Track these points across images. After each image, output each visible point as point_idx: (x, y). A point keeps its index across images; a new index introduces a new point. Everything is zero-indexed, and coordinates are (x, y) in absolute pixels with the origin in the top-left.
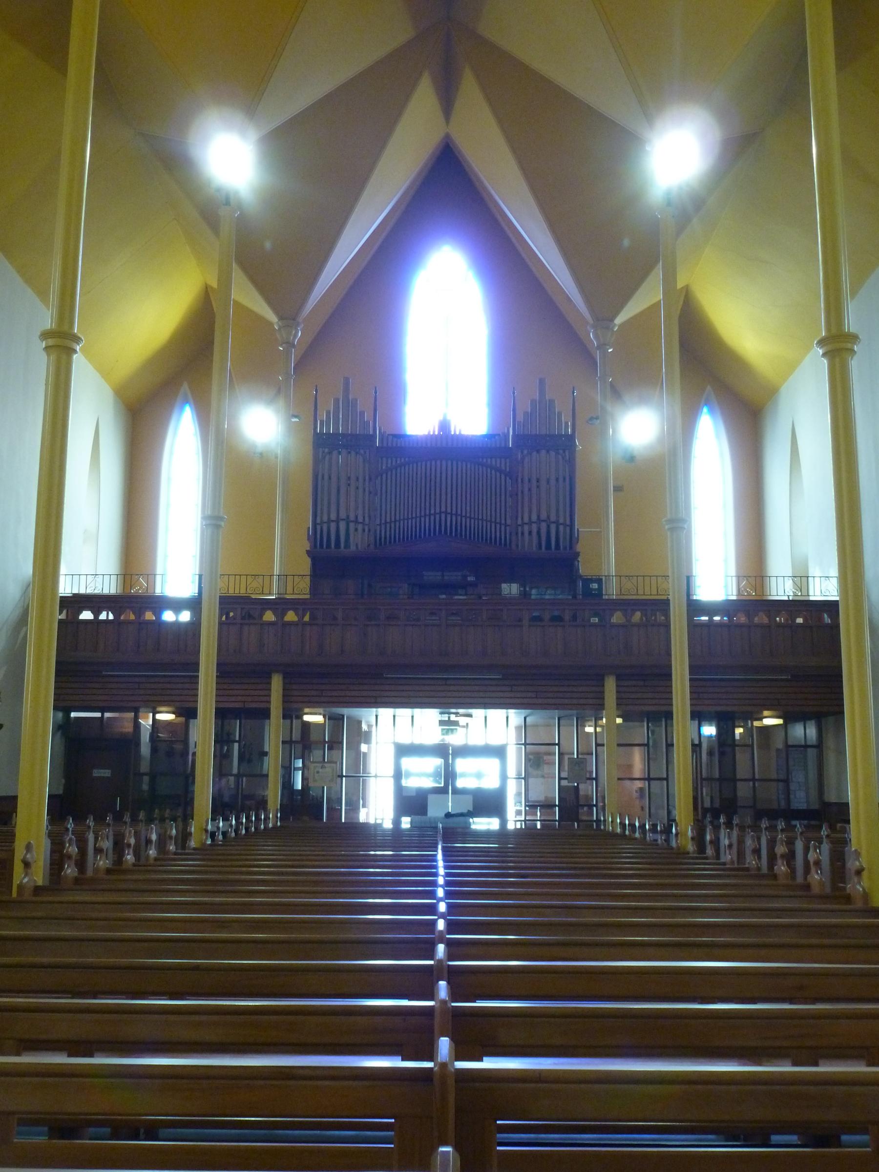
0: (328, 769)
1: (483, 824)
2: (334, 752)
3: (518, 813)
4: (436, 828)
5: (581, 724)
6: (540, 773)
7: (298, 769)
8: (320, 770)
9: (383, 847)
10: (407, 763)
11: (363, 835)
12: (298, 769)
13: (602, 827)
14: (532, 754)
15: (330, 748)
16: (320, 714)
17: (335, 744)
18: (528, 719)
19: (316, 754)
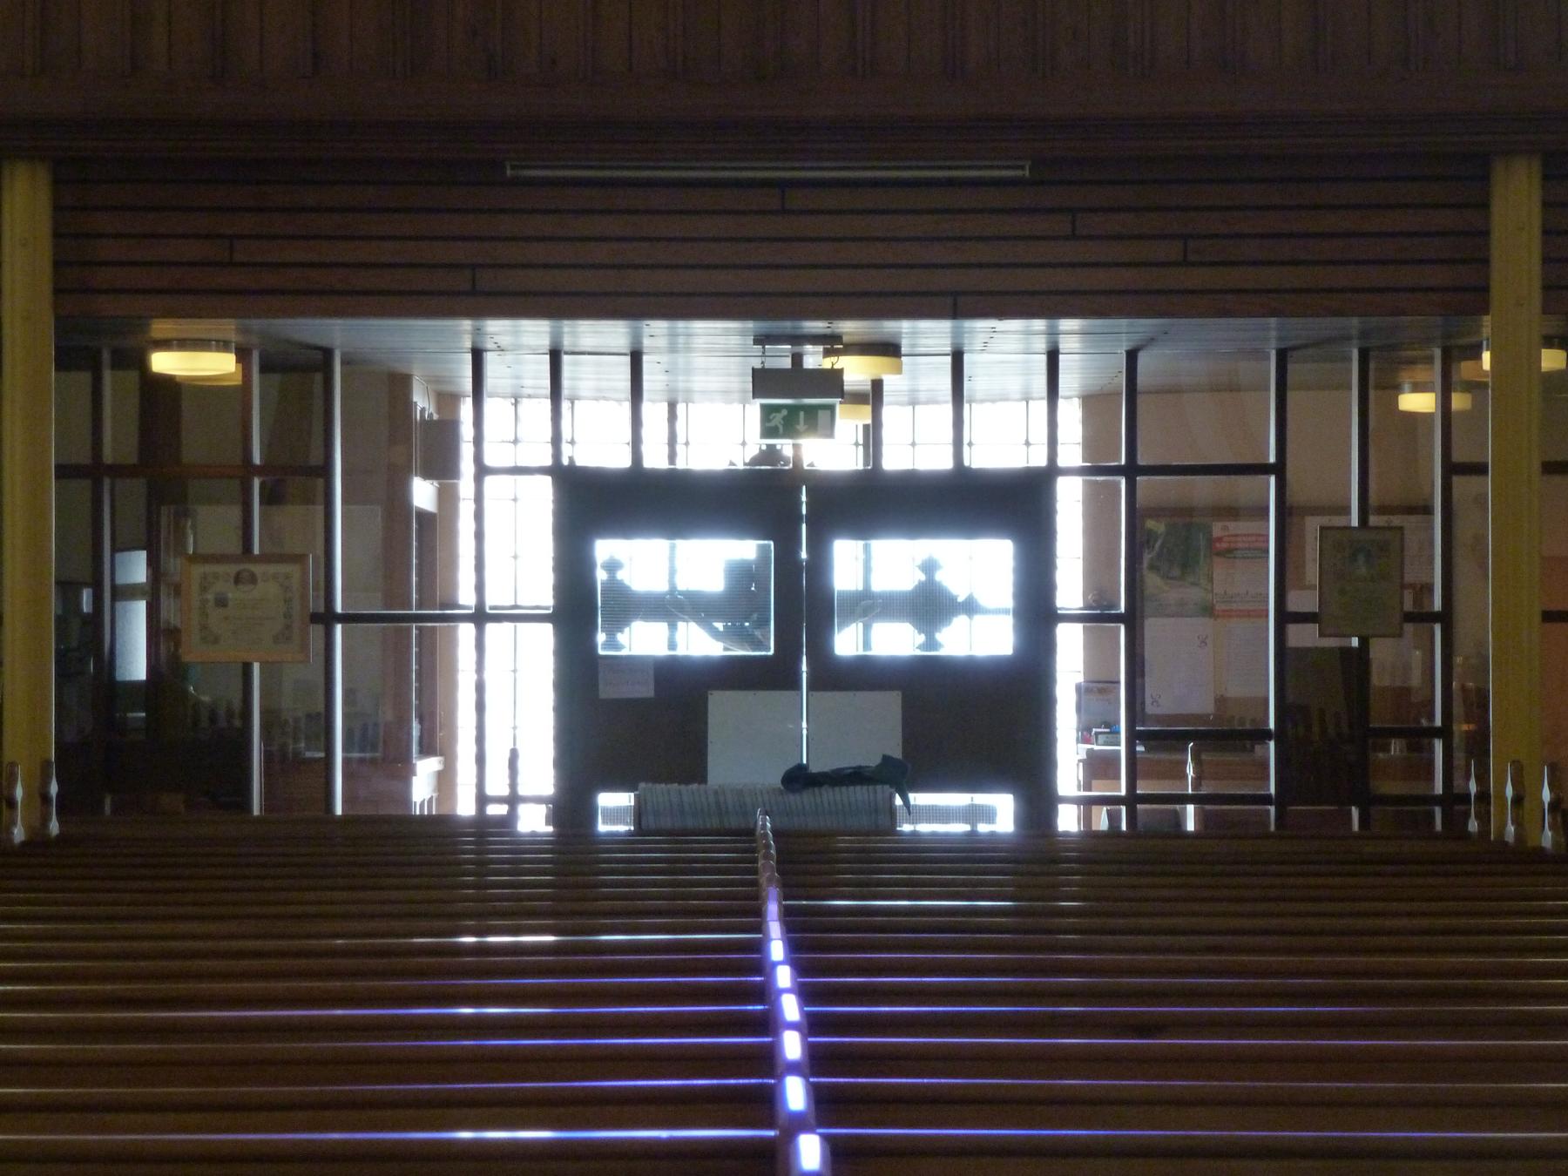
0: (268, 586)
1: (944, 813)
2: (290, 514)
3: (1098, 767)
4: (749, 833)
5: (1377, 383)
6: (1194, 594)
7: (131, 592)
8: (233, 594)
9: (519, 916)
10: (635, 560)
11: (453, 864)
12: (131, 592)
13: (1473, 826)
14: (1157, 512)
15: (272, 498)
16: (223, 346)
17: (296, 476)
18: (1143, 360)
19: (212, 525)
